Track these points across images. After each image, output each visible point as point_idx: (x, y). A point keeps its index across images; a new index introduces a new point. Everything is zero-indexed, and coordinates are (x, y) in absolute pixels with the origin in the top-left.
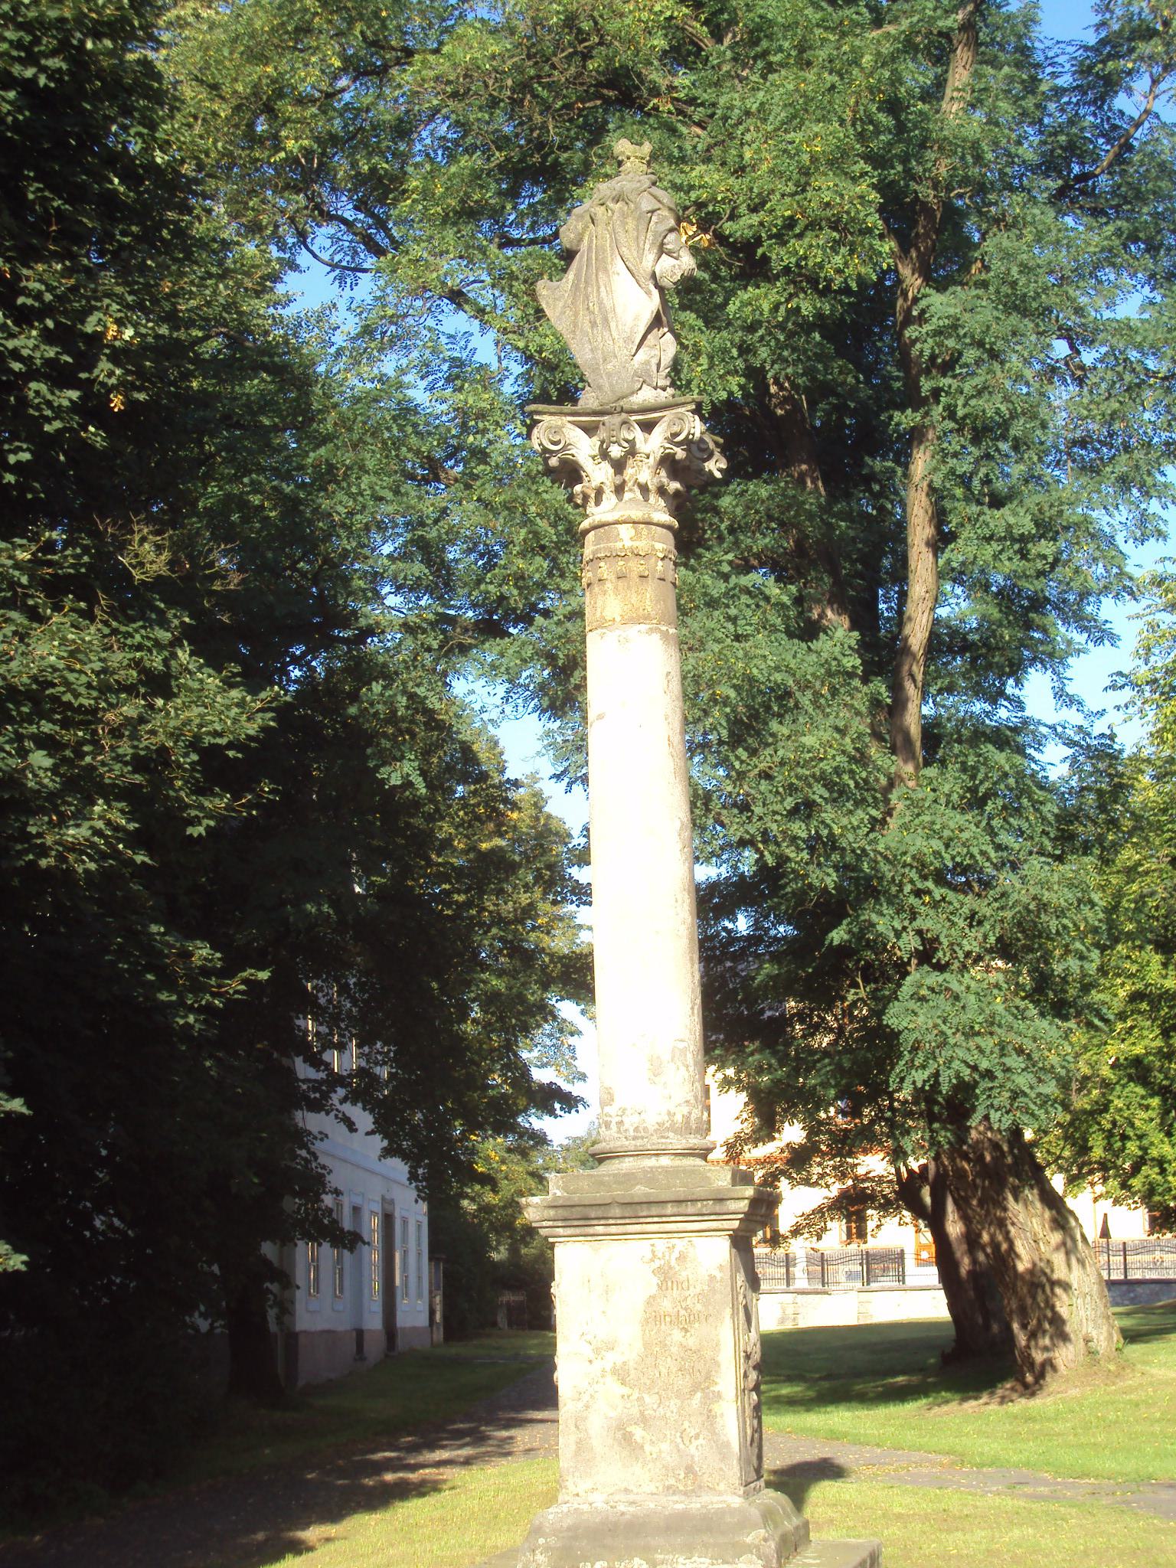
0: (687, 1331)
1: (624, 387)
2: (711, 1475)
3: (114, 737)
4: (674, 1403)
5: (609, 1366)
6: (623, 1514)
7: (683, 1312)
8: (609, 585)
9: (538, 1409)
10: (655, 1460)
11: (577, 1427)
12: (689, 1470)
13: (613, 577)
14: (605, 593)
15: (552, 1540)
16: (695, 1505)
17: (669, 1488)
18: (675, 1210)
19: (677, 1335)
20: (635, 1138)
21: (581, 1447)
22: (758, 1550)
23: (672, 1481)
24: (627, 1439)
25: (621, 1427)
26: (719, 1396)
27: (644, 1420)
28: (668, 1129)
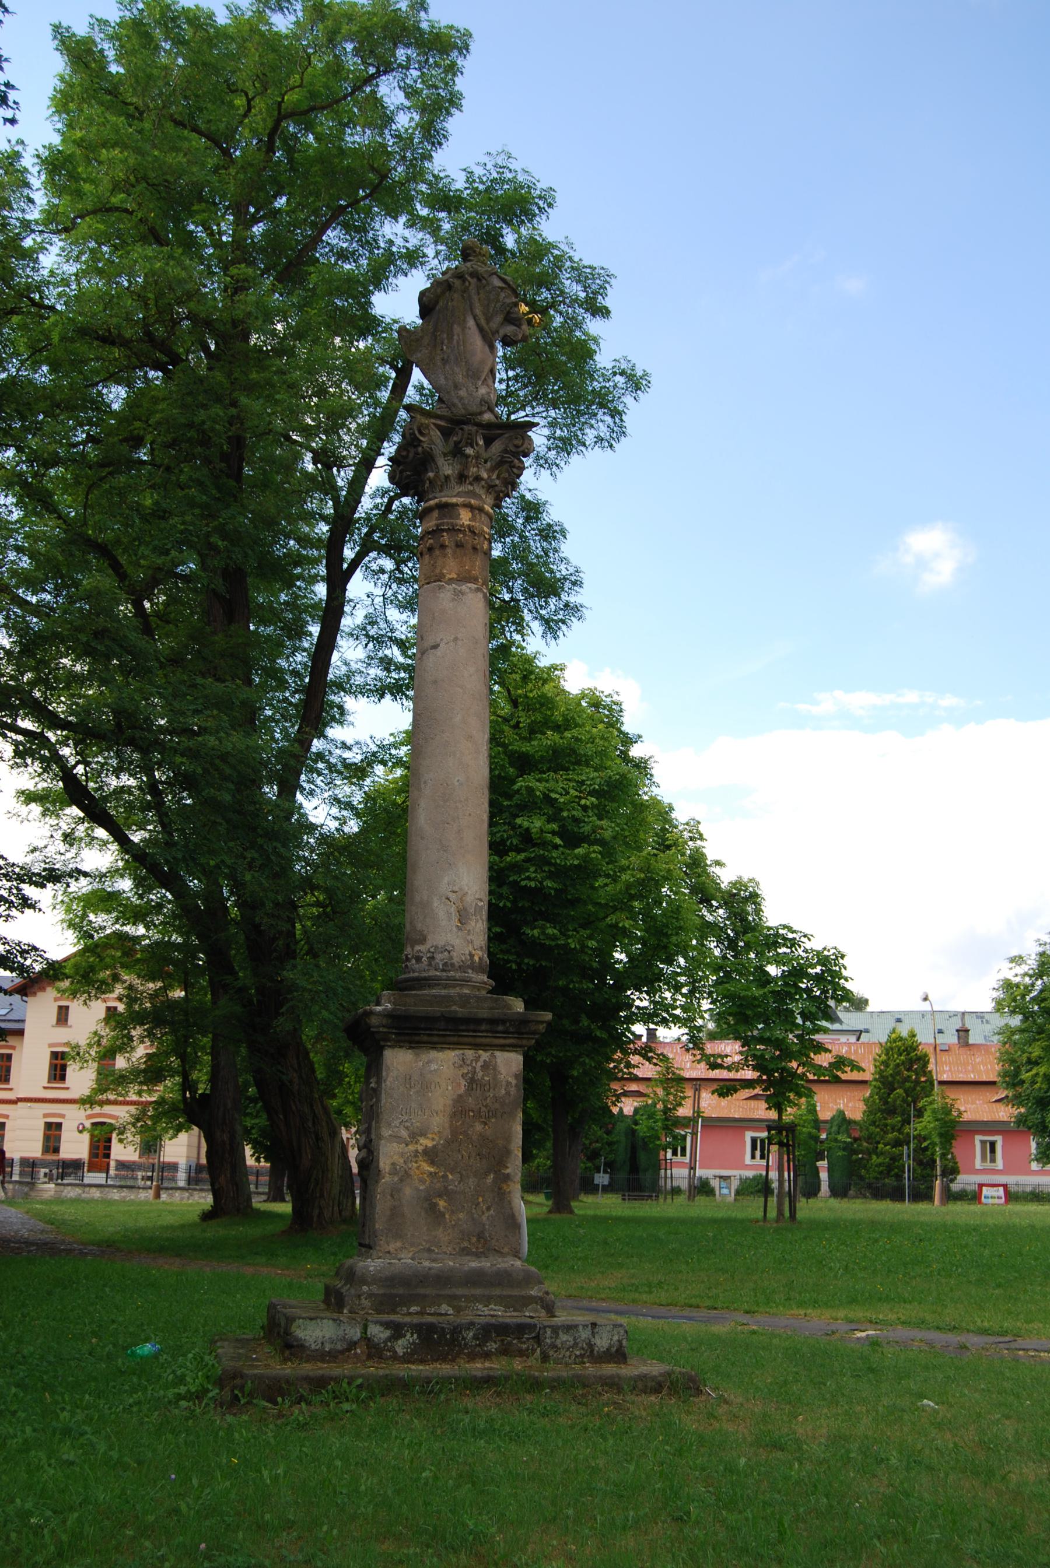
0: (486, 1124)
1: (474, 408)
2: (498, 1240)
3: (545, 538)
4: (472, 1182)
5: (420, 1148)
6: (430, 1269)
7: (483, 1109)
8: (449, 551)
9: (1003, 1158)
10: (454, 1226)
11: (392, 1196)
12: (480, 1236)
13: (453, 545)
14: (445, 556)
15: (375, 1289)
16: (485, 1264)
17: (464, 1249)
18: (488, 1027)
19: (479, 1127)
20: (443, 970)
21: (395, 1213)
22: (542, 1301)
23: (466, 1244)
24: (433, 1207)
25: (427, 1199)
26: (507, 1178)
27: (446, 1193)
28: (469, 967)
